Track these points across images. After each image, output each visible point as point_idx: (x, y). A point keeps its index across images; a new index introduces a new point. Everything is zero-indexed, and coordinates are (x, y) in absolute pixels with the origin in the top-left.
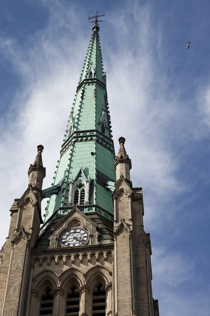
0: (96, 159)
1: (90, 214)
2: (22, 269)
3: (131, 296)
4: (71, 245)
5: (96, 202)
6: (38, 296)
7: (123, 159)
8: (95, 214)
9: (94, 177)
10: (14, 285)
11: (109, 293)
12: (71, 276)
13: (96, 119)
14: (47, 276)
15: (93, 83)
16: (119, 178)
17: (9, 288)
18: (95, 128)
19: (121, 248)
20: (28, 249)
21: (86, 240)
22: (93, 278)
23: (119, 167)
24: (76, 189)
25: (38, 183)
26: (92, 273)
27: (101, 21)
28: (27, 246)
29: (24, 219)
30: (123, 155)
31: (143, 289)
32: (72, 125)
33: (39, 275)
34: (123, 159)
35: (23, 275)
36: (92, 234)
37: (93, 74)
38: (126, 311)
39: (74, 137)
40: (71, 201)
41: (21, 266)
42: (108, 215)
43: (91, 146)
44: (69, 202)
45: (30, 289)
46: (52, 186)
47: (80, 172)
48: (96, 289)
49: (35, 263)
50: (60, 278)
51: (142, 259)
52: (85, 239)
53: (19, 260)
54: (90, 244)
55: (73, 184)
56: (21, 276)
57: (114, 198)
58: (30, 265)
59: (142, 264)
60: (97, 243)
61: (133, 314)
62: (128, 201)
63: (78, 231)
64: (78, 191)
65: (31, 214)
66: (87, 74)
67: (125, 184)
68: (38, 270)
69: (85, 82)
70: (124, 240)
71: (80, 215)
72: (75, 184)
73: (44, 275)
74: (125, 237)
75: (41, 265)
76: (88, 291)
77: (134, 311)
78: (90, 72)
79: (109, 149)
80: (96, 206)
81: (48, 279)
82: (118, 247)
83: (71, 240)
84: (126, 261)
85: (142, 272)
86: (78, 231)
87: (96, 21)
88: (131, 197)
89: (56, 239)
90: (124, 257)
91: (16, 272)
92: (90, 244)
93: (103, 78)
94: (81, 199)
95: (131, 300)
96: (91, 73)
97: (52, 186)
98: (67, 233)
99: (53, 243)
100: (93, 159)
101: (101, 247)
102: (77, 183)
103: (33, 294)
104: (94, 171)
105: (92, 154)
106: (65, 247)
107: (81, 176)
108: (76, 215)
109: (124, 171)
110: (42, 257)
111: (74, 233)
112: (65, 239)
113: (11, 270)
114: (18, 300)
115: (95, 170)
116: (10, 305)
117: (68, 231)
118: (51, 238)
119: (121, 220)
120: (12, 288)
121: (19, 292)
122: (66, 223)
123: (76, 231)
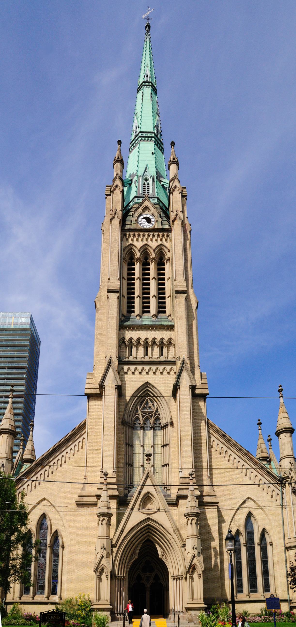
4: (145, 227)
6: (126, 262)
7: (174, 161)
8: (157, 204)
12: (145, 250)
21: (153, 223)
24: (143, 182)
32: (137, 126)
38: (180, 278)
39: (140, 137)
41: (117, 238)
42: (164, 206)
44: (140, 192)
64: (144, 184)
70: (178, 227)
71: (149, 204)
74: (179, 224)
76: (155, 262)
84: (179, 242)
87: (148, 18)
101: (162, 230)
110: (128, 233)
112: (140, 221)
116: (113, 266)
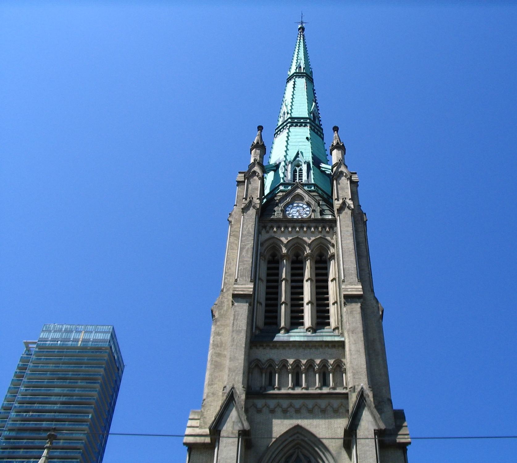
0: (311, 143)
1: (310, 191)
2: (253, 233)
3: (356, 266)
5: (314, 181)
7: (259, 145)
9: (311, 160)
10: (247, 247)
11: (332, 262)
13: (308, 108)
14: (321, 243)
15: (303, 77)
16: (253, 161)
17: (242, 249)
18: (307, 116)
19: (344, 223)
20: (257, 216)
22: (316, 247)
23: (335, 152)
24: (294, 168)
25: (261, 159)
26: (316, 243)
27: (306, 23)
28: (256, 214)
29: (251, 189)
30: (339, 141)
31: (364, 261)
33: (266, 240)
34: (259, 145)
35: (254, 239)
36: (314, 208)
37: (302, 68)
39: (289, 122)
40: (291, 178)
41: (252, 231)
43: (306, 131)
45: (259, 253)
46: (268, 164)
47: (298, 154)
48: (294, 258)
49: (262, 229)
50: (287, 245)
51: (362, 235)
52: (308, 213)
53: (250, 226)
54: (313, 217)
55: (292, 163)
56: (252, 239)
57: (246, 178)
58: (258, 232)
59: (362, 239)
60: (319, 217)
61: (358, 282)
62: (347, 182)
63: (301, 205)
65: (256, 186)
66: (297, 68)
67: (343, 168)
68: (265, 236)
69: (295, 74)
72: (293, 163)
73: (271, 241)
75: (267, 232)
76: (312, 259)
77: (359, 279)
78: (299, 66)
79: (320, 136)
80: (314, 185)
81: (275, 245)
82: (341, 222)
83: (295, 212)
84: (349, 235)
85: (362, 246)
86: (301, 205)
88: (261, 179)
89: (281, 210)
90: (347, 231)
91: (247, 236)
92: (313, 217)
93: (310, 73)
94: (299, 177)
95: (356, 269)
96: (300, 67)
97: (268, 164)
98: (291, 206)
99: (278, 214)
100: (308, 144)
102: (295, 163)
103: (262, 257)
104: (310, 154)
105: (307, 138)
106: (289, 217)
107: (298, 157)
108: (299, 191)
109: (340, 156)
111: (298, 206)
112: (289, 211)
113: (242, 234)
114: (251, 261)
115: (311, 154)
116: (244, 264)
117: (292, 204)
118: (276, 209)
119: (250, 198)
120: (245, 250)
121: (252, 253)
122: (289, 198)
123: (299, 204)
